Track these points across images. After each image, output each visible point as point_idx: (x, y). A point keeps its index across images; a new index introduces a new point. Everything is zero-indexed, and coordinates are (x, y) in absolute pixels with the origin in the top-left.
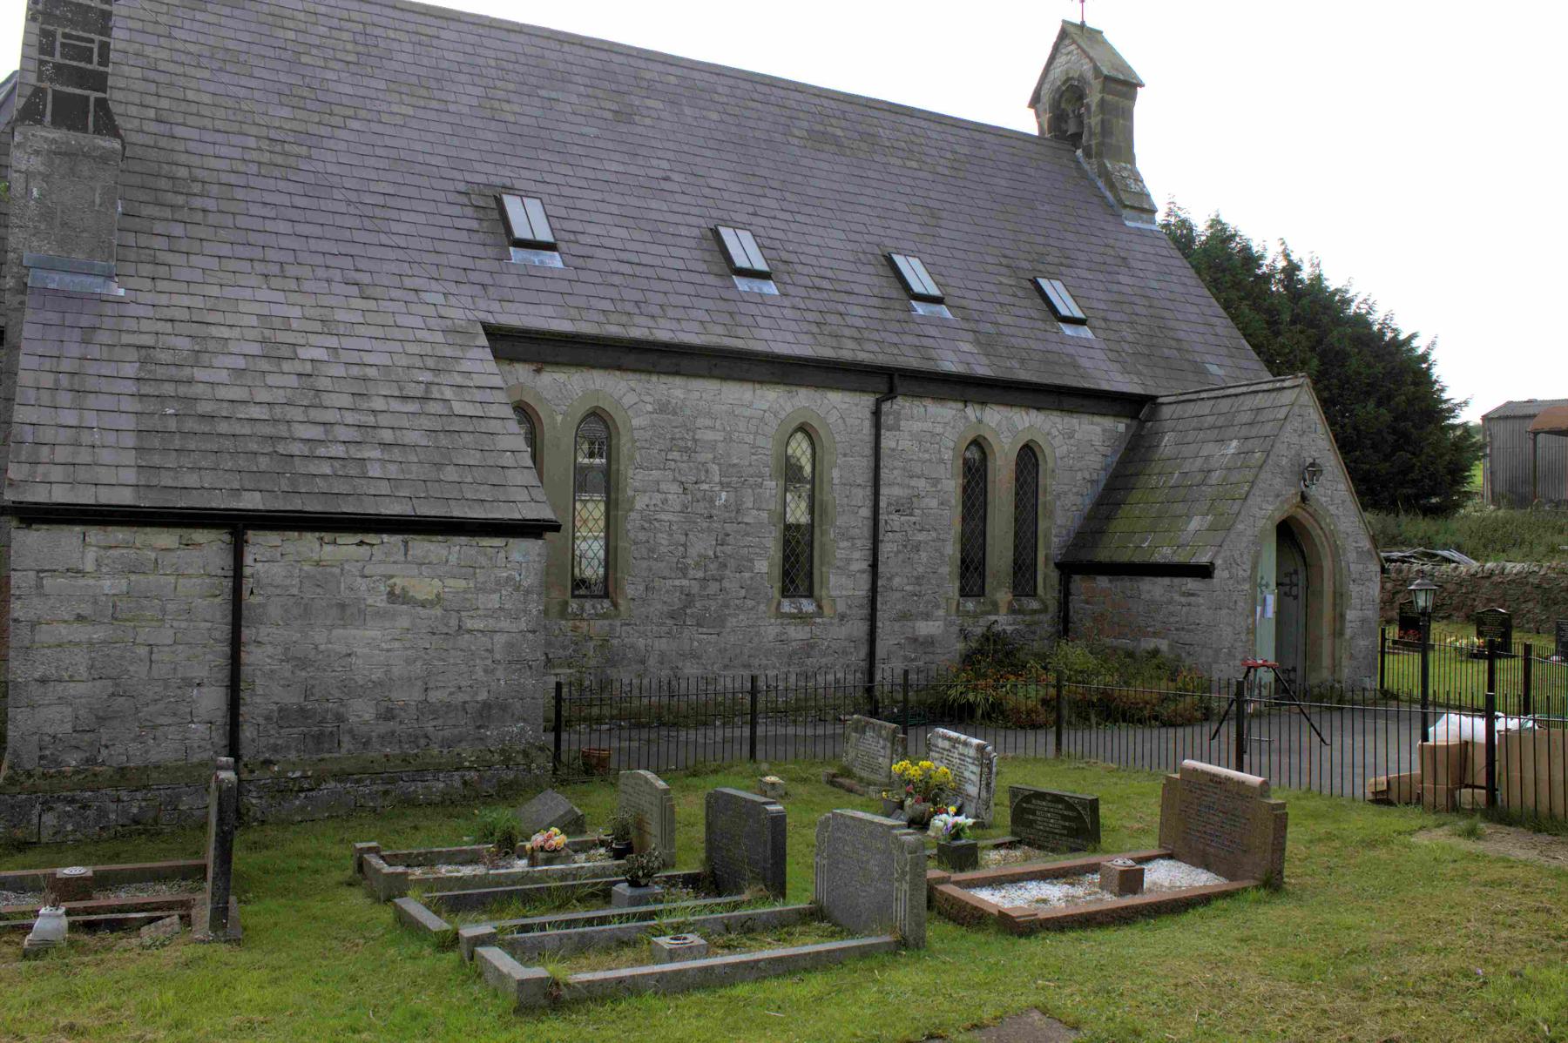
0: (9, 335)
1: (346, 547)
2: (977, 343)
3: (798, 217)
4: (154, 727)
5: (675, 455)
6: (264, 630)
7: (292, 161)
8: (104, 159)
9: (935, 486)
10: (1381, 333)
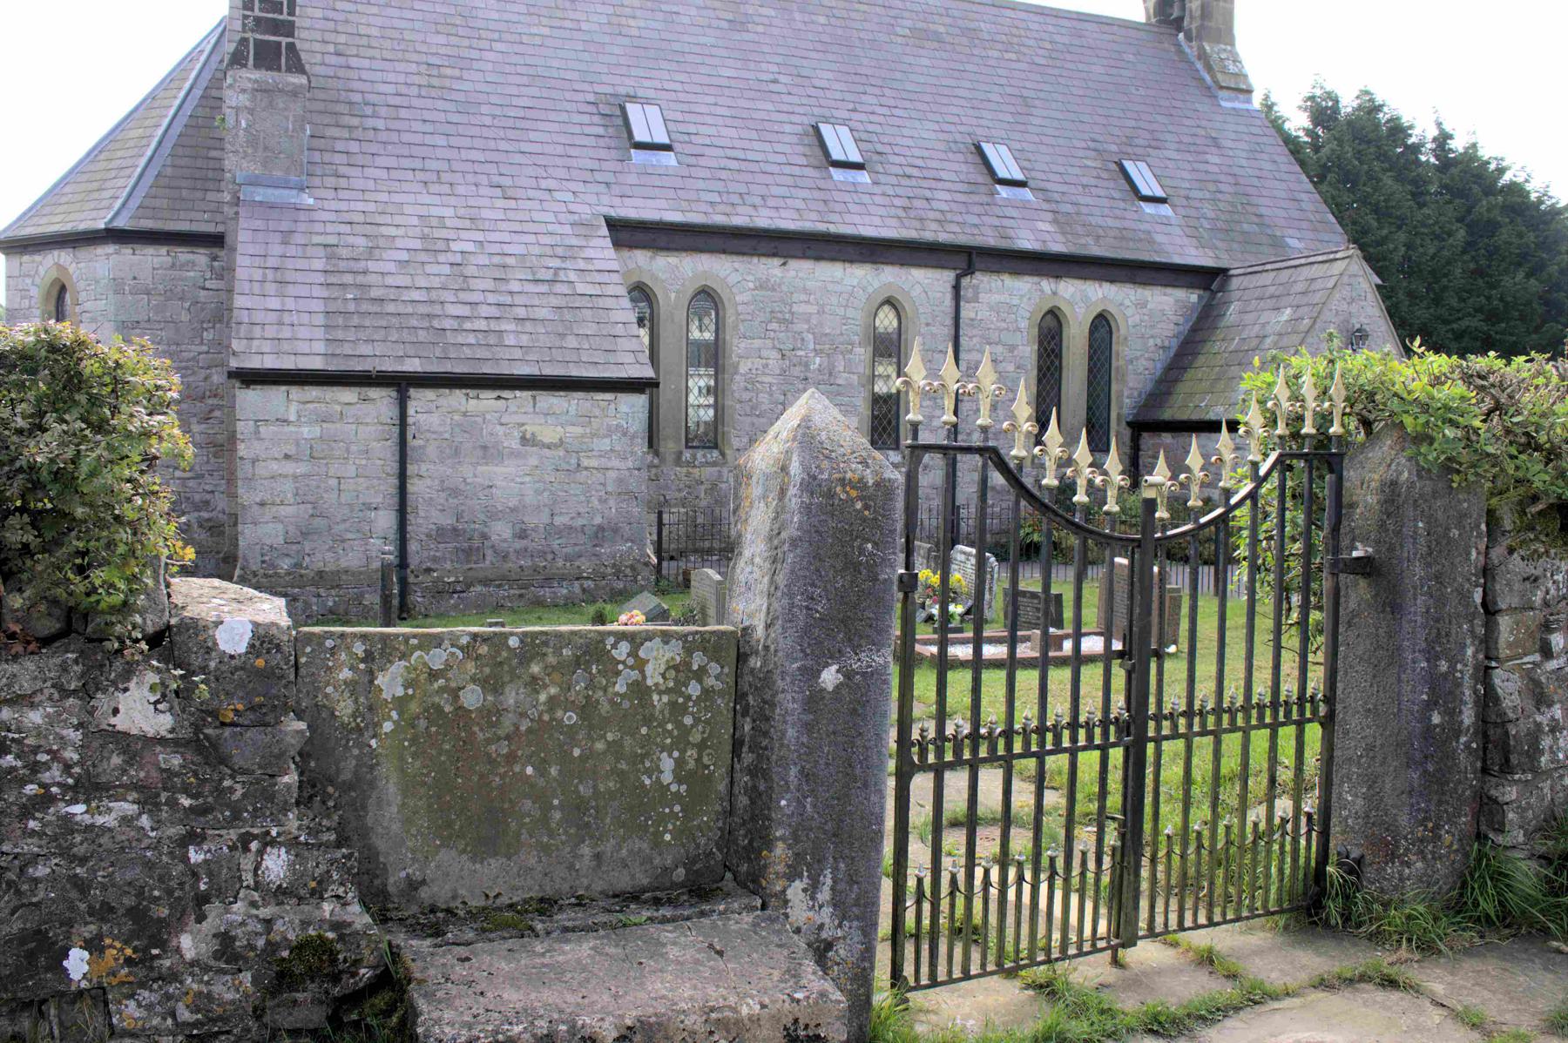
0: (228, 240)
1: (487, 401)
2: (1055, 221)
3: (897, 112)
4: (343, 541)
5: (774, 326)
6: (424, 467)
7: (447, 83)
8: (295, 93)
9: (1011, 351)
10: (1540, 201)
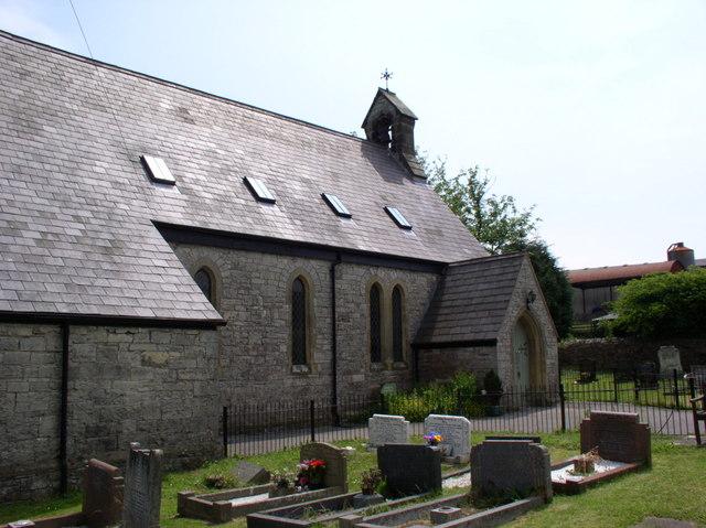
1: (120, 336)
